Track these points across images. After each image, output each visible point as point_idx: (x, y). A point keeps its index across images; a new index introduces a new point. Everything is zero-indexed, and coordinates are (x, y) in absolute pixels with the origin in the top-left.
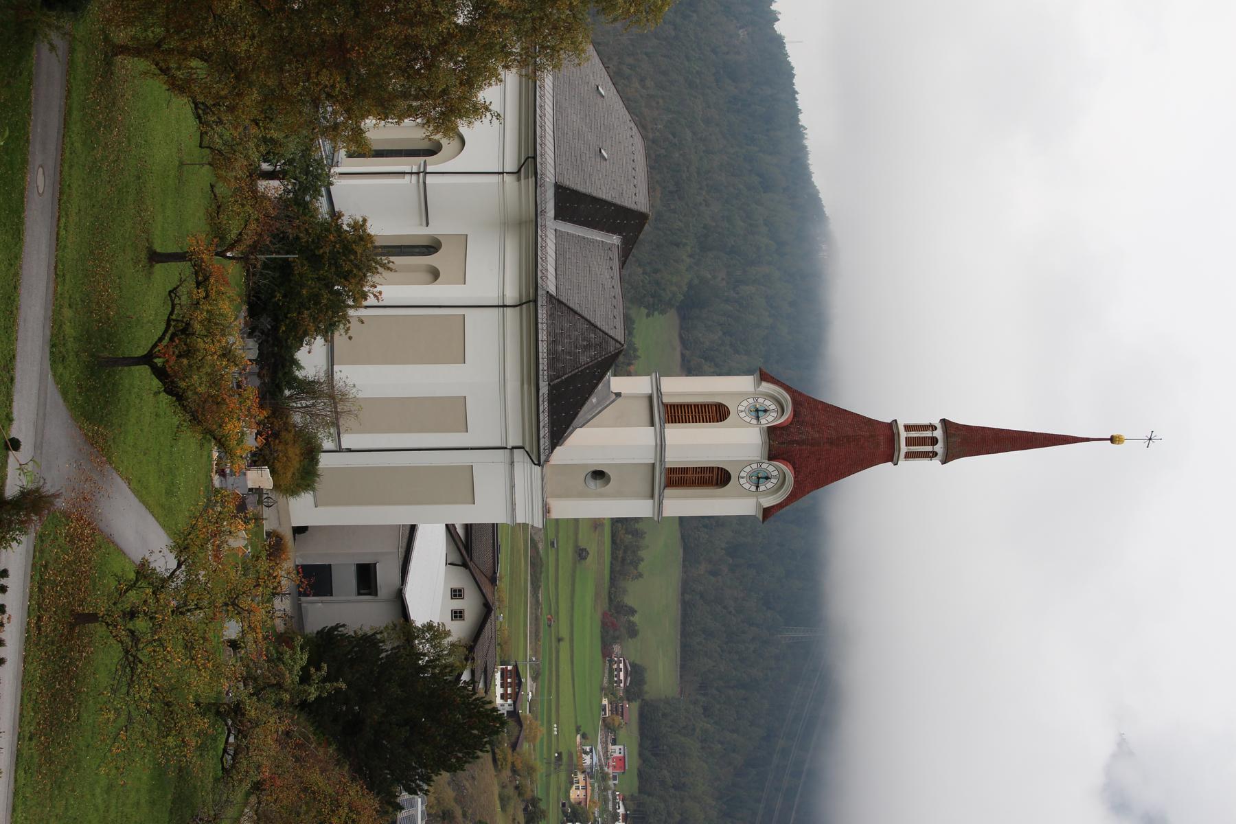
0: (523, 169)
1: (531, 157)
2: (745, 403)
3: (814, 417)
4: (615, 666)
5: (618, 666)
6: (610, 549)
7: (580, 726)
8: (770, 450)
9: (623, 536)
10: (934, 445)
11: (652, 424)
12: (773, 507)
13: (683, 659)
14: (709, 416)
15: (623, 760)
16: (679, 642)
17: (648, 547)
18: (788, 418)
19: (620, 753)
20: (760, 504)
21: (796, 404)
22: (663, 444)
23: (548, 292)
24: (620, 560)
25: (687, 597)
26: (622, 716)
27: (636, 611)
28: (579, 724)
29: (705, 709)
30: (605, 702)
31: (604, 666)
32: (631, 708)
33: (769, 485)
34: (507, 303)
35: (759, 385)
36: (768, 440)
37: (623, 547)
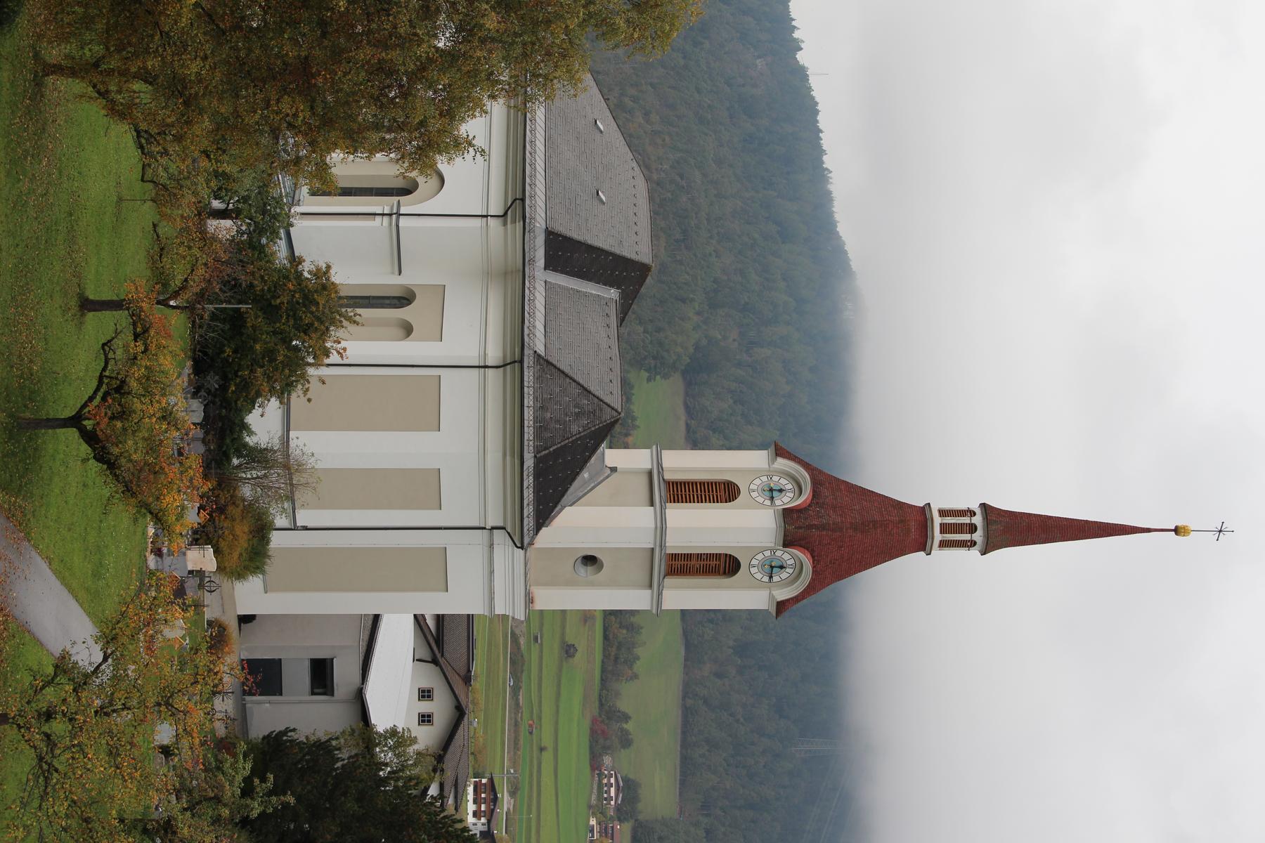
0: (509, 212)
2: (757, 482)
4: (605, 781)
5: (609, 780)
9: (616, 631)
11: (652, 504)
12: (788, 600)
16: (679, 753)
18: (806, 500)
20: (773, 597)
21: (816, 483)
22: (664, 526)
23: (535, 352)
24: (612, 658)
25: (689, 702)
26: (612, 839)
27: (630, 718)
29: (708, 832)
30: (593, 822)
33: (784, 575)
37: (616, 644)
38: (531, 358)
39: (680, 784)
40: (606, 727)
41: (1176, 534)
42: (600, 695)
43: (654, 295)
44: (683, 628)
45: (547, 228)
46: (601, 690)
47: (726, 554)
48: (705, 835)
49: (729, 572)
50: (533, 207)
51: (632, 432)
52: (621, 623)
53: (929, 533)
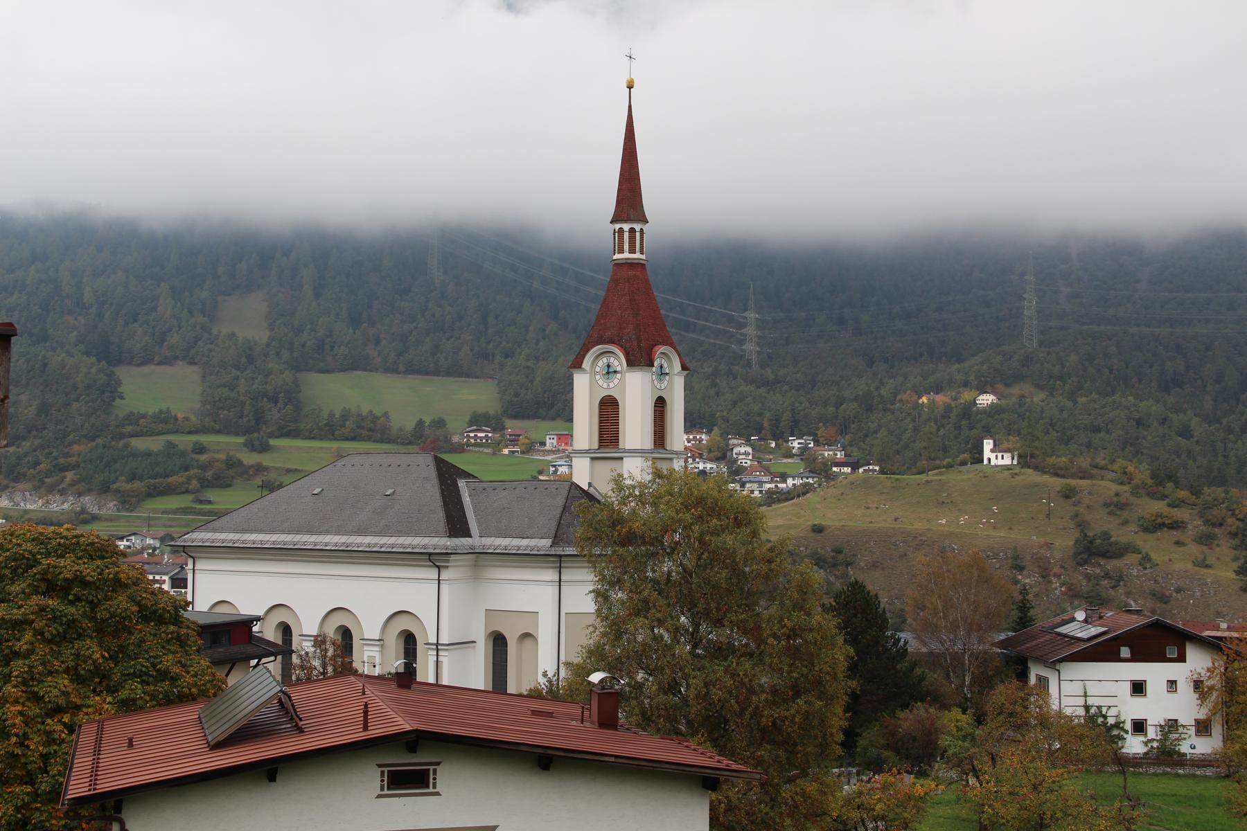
2: (601, 382)
3: (613, 327)
4: (472, 441)
6: (360, 443)
9: (348, 430)
11: (621, 458)
13: (460, 375)
15: (560, 436)
16: (444, 378)
17: (358, 406)
19: (553, 439)
20: (679, 373)
21: (601, 341)
23: (551, 546)
24: (370, 433)
25: (401, 368)
26: (519, 435)
28: (530, 477)
29: (507, 356)
30: (506, 451)
31: (472, 451)
32: (512, 426)
33: (665, 365)
35: (584, 370)
37: (358, 430)
40: (429, 440)
41: (632, 87)
42: (402, 444)
43: (42, 391)
44: (339, 372)
46: (397, 443)
51: (173, 414)
52: (341, 426)
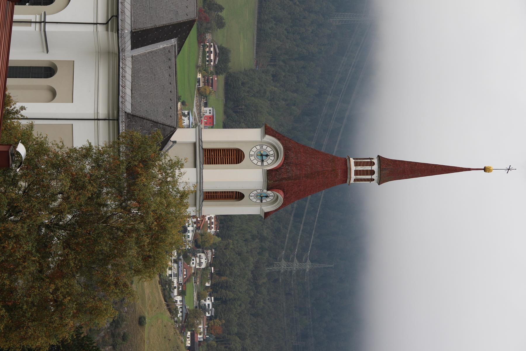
0: (110, 22)
1: (115, 16)
2: (254, 149)
4: (207, 50)
5: (210, 49)
7: (181, 96)
8: (268, 186)
10: (372, 175)
11: (195, 166)
12: (271, 212)
14: (232, 158)
18: (280, 164)
19: (210, 113)
20: (263, 210)
21: (287, 149)
22: (201, 181)
23: (126, 112)
26: (212, 86)
27: (223, 9)
28: (180, 95)
29: (274, 76)
30: (199, 76)
31: (199, 50)
33: (268, 200)
34: (100, 117)
36: (266, 181)
38: (123, 117)
39: (256, 46)
45: (132, 31)
47: (236, 192)
48: (272, 78)
49: (238, 198)
50: (123, 21)
53: (348, 176)
